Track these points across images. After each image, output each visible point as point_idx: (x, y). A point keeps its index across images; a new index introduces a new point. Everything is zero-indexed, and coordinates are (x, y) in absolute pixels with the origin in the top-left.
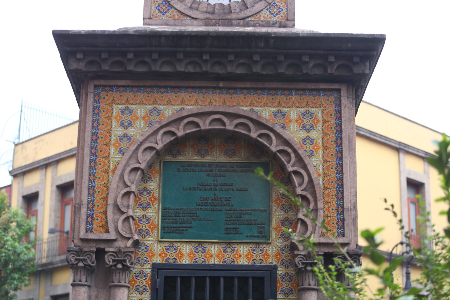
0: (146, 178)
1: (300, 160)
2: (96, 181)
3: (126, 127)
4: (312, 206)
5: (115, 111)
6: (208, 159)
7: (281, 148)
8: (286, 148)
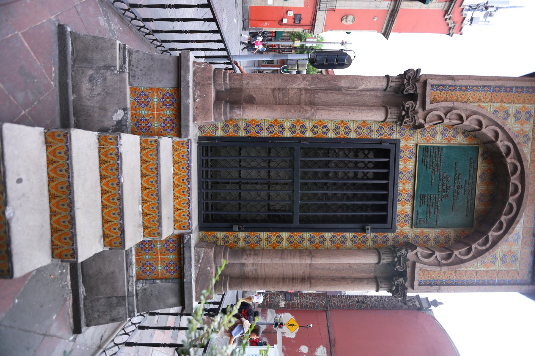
0: (466, 133)
1: (480, 253)
2: (472, 92)
3: (515, 116)
4: (444, 262)
5: (529, 106)
6: (478, 181)
7: (491, 239)
8: (490, 243)
